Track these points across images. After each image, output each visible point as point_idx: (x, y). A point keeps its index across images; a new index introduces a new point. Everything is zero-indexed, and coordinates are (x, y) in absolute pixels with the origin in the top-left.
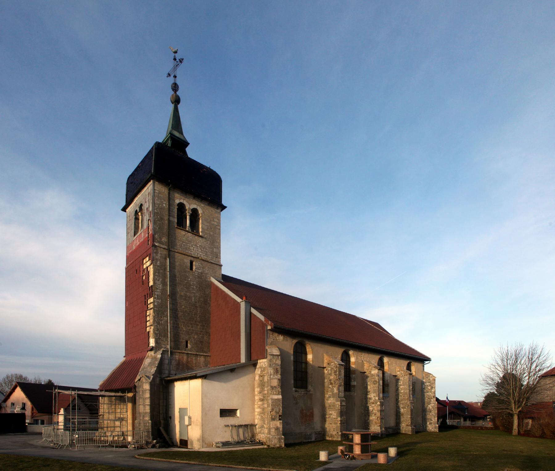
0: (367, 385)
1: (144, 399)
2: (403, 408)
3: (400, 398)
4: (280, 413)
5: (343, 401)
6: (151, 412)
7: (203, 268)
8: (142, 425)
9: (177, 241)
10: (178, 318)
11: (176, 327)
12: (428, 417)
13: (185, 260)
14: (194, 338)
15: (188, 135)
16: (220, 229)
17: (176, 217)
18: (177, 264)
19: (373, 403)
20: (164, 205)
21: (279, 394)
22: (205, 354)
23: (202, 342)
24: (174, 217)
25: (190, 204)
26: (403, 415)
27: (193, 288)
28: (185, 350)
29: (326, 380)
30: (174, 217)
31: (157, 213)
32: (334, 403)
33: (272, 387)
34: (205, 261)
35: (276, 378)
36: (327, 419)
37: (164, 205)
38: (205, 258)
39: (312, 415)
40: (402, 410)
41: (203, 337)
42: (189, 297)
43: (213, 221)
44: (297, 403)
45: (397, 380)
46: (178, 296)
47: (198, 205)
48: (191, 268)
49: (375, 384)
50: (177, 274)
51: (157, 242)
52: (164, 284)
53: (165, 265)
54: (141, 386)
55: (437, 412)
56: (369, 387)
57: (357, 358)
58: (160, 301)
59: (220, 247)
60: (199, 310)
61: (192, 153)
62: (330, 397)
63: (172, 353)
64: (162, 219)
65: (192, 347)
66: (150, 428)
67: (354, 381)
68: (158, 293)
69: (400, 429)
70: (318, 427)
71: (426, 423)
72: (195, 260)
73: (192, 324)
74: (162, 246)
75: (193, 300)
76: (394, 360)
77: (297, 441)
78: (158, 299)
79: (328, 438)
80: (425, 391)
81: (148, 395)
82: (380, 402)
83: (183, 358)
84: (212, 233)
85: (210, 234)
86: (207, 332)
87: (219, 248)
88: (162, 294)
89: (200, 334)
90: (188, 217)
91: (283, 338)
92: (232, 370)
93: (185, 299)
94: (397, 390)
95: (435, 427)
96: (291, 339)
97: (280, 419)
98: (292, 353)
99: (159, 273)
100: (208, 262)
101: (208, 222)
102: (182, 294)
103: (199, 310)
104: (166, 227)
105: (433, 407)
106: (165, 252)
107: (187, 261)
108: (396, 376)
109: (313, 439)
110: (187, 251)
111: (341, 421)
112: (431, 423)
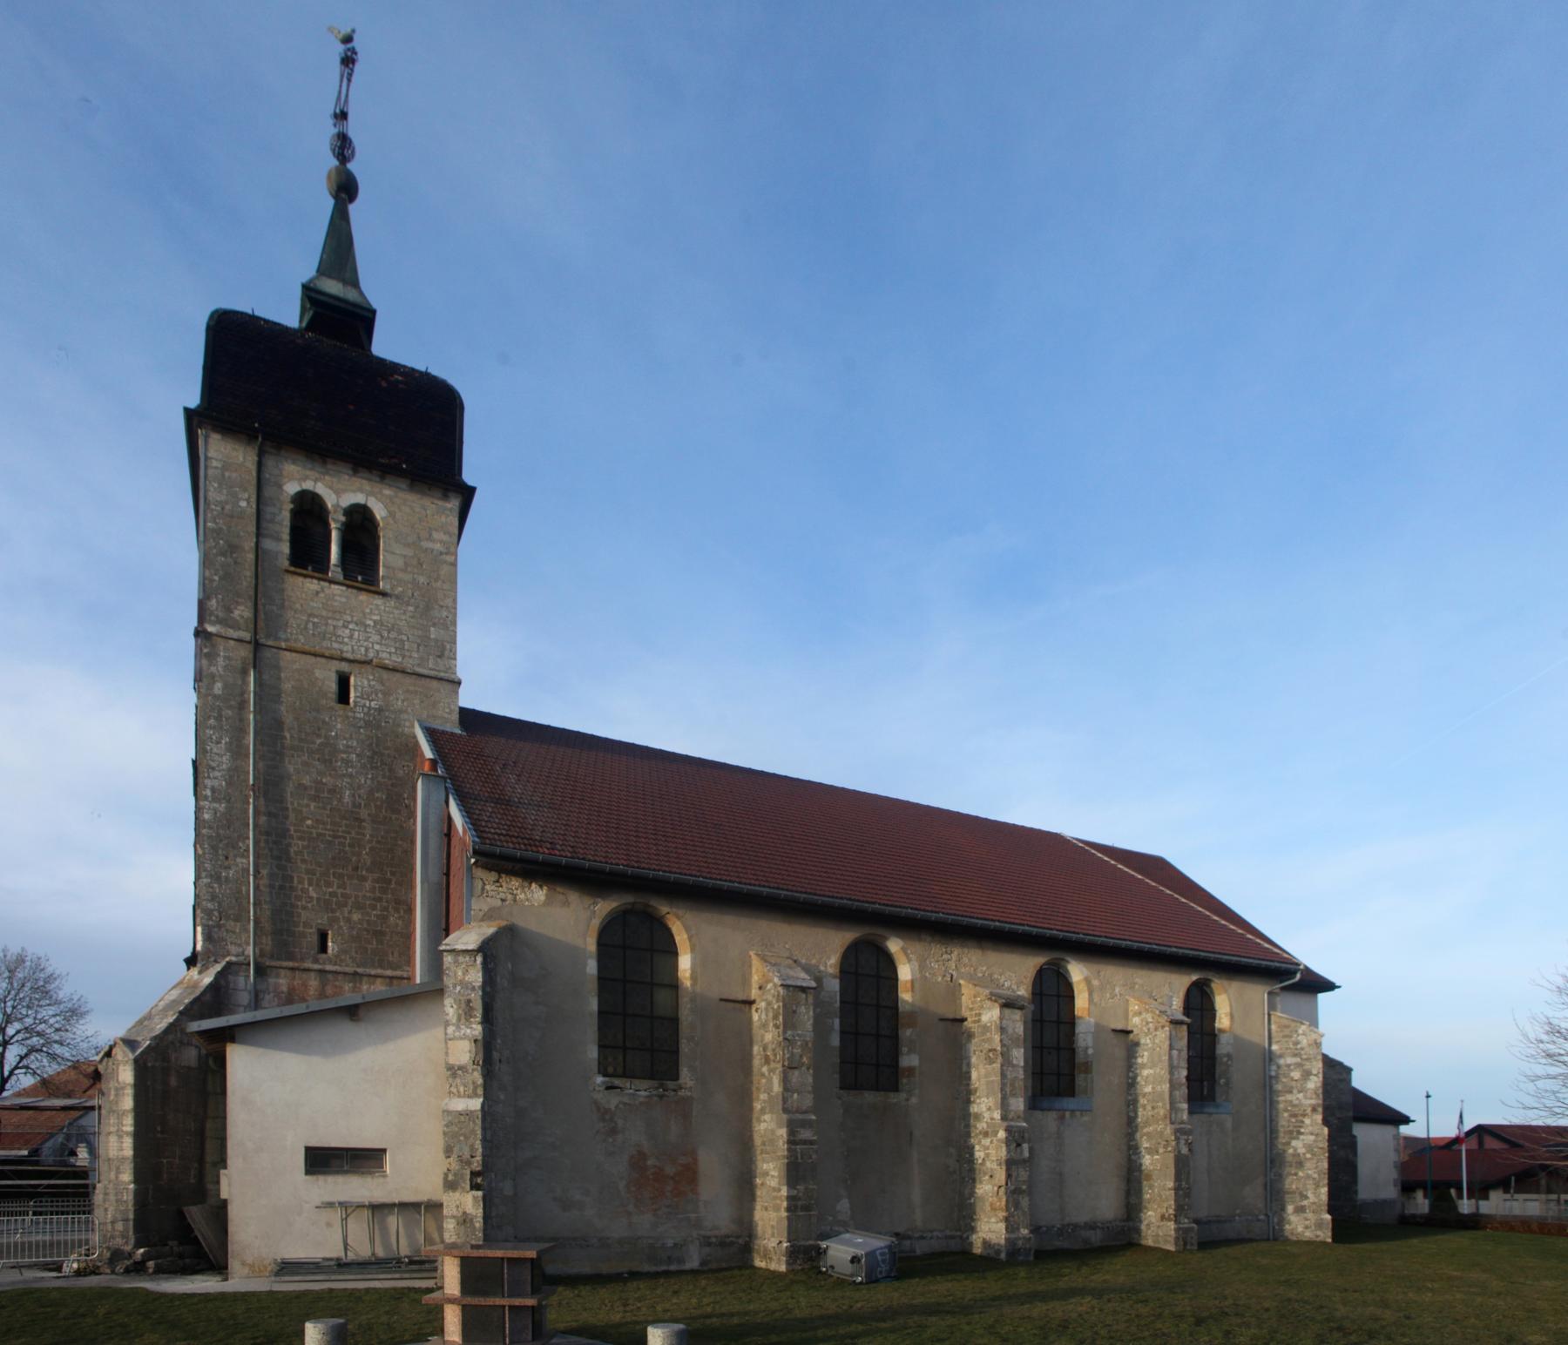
0: (969, 1065)
1: (120, 1115)
2: (1151, 1151)
3: (1142, 1115)
4: (477, 1164)
5: (805, 1124)
6: (135, 1156)
7: (386, 694)
8: (112, 1197)
9: (290, 614)
10: (289, 860)
11: (282, 887)
12: (1291, 1184)
13: (318, 673)
14: (348, 920)
15: (377, 284)
16: (454, 564)
17: (286, 536)
18: (287, 686)
19: (986, 1134)
20: (243, 504)
21: (475, 1095)
22: (389, 973)
23: (379, 934)
24: (279, 539)
25: (338, 493)
26: (1149, 1177)
27: (347, 762)
28: (316, 961)
29: (756, 1049)
30: (279, 539)
31: (218, 532)
32: (773, 1132)
33: (450, 1068)
34: (394, 670)
35: (465, 1037)
36: (758, 1193)
37: (243, 504)
38: (389, 657)
39: (689, 1175)
40: (1147, 1161)
41: (384, 918)
42: (333, 791)
43: (430, 538)
44: (613, 1131)
45: (1132, 1048)
46: (290, 788)
47: (368, 494)
48: (343, 697)
49: (991, 1062)
50: (288, 719)
51: (213, 623)
52: (238, 751)
53: (243, 692)
54: (115, 1073)
55: (1326, 1165)
56: (974, 1075)
57: (922, 967)
58: (222, 807)
59: (454, 623)
60: (368, 833)
61: (391, 343)
62: (763, 1111)
63: (261, 971)
64: (232, 548)
65: (343, 951)
66: (131, 1207)
67: (910, 1051)
68: (216, 783)
69: (1138, 1231)
70: (717, 1216)
71: (1283, 1209)
72: (355, 669)
73: (341, 876)
74: (231, 633)
75: (347, 799)
76: (1117, 976)
77: (605, 1269)
78: (214, 800)
79: (759, 1263)
80: (1279, 1087)
81: (128, 1103)
82: (1008, 1130)
83: (305, 985)
84: (422, 579)
85: (415, 583)
86: (398, 902)
87: (449, 625)
88: (229, 784)
89: (374, 908)
90: (334, 535)
91: (549, 902)
92: (352, 1012)
93: (316, 798)
94: (1131, 1084)
95: (1319, 1225)
96: (588, 901)
97: (475, 1187)
98: (591, 945)
99: (219, 718)
100: (403, 672)
101: (408, 545)
102: (306, 780)
103: (368, 833)
104: (248, 572)
105: (1309, 1148)
106: (245, 652)
107: (327, 678)
108: (1128, 1032)
109: (693, 1263)
110: (326, 644)
111: (789, 1198)
112: (1300, 1210)
